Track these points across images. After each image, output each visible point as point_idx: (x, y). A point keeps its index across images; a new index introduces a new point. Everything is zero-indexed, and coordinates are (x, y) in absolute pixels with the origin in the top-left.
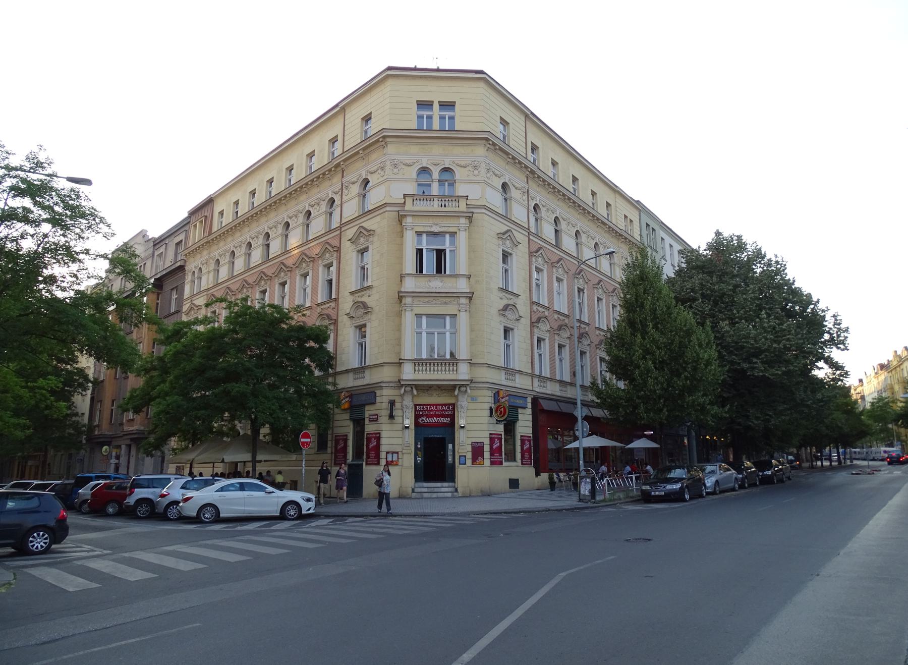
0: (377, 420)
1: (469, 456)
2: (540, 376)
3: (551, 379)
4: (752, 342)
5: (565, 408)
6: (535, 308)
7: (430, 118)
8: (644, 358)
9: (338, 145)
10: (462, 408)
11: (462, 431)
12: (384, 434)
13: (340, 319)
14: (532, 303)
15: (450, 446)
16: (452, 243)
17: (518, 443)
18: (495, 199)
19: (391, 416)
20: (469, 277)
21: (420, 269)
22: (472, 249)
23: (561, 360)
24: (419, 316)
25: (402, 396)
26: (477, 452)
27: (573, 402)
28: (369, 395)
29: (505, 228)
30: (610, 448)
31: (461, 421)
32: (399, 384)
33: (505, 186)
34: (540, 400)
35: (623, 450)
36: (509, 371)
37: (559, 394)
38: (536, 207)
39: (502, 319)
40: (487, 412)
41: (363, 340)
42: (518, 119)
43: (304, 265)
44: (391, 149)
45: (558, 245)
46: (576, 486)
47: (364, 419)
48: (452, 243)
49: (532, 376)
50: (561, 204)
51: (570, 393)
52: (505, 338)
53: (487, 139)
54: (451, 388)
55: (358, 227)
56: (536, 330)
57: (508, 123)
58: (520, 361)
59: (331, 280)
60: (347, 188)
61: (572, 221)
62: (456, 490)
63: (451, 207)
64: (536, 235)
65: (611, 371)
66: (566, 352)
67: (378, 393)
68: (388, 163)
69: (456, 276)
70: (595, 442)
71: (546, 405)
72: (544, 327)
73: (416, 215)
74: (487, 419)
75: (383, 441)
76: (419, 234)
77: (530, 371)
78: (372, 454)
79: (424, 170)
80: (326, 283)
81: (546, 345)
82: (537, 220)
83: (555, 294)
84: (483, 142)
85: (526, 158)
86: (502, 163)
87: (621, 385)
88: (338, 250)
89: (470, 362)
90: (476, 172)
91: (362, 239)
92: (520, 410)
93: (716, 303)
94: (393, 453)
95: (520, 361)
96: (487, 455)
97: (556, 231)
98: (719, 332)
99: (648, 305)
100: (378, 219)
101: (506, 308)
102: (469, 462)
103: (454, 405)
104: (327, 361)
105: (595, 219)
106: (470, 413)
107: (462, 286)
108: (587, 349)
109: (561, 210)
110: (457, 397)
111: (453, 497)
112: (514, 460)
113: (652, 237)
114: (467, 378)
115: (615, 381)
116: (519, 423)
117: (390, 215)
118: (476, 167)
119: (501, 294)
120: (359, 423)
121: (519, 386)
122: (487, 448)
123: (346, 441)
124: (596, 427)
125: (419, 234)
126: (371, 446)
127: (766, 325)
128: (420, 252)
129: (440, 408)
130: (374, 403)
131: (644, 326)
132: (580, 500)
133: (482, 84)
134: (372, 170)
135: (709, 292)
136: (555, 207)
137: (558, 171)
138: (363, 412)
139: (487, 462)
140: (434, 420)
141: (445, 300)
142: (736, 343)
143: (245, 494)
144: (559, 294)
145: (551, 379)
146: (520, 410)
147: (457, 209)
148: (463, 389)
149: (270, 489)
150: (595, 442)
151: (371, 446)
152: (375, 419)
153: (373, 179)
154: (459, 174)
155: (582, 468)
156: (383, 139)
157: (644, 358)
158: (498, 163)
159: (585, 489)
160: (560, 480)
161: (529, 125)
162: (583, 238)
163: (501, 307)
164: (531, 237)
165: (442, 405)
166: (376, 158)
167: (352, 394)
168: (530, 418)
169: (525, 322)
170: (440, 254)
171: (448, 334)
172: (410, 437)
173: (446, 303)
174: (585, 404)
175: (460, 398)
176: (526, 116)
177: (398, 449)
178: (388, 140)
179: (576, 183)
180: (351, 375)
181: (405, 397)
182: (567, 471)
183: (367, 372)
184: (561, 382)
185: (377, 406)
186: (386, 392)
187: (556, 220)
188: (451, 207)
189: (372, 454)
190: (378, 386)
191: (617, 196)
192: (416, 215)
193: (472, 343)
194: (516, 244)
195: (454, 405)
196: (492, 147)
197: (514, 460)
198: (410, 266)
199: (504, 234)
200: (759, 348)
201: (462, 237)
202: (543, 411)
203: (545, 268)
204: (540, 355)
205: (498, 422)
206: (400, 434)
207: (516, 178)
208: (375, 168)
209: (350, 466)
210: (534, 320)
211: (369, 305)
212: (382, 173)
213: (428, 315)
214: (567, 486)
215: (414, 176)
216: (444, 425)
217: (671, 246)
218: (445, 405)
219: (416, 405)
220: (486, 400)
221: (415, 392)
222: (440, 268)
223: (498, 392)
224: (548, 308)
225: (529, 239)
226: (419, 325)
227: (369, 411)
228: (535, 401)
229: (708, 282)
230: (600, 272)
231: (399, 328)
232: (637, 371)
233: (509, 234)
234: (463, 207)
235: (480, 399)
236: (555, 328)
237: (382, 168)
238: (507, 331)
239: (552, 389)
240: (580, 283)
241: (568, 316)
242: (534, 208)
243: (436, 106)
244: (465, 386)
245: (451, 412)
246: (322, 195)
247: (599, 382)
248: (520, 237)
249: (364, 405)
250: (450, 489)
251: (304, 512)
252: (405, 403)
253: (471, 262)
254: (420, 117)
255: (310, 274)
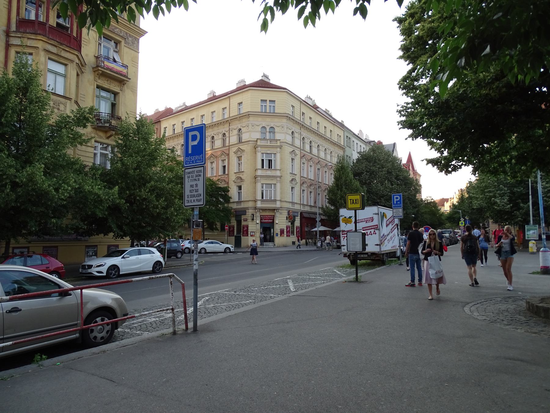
0: (247, 220)
1: (279, 233)
2: (303, 204)
3: (307, 205)
4: (381, 192)
5: (312, 216)
6: (302, 179)
7: (265, 106)
8: (341, 199)
9: (227, 111)
10: (277, 216)
11: (277, 225)
12: (249, 226)
13: (230, 182)
14: (301, 177)
15: (272, 230)
16: (275, 157)
17: (295, 229)
18: (289, 139)
19: (253, 219)
20: (280, 170)
21: (263, 167)
22: (281, 159)
23: (310, 197)
24: (262, 184)
25: (256, 212)
26: (282, 232)
27: (315, 214)
28: (244, 212)
29: (293, 149)
30: (138, 37)
31: (277, 221)
32: (255, 208)
33: (293, 132)
34: (303, 213)
35: (332, 231)
36: (293, 203)
37: (309, 211)
38: (303, 138)
39: (291, 184)
40: (286, 218)
41: (240, 191)
42: (297, 104)
43: (212, 158)
44: (251, 119)
45: (311, 153)
46: (315, 244)
47: (241, 220)
48: (275, 157)
49: (300, 204)
50: (313, 135)
51: (314, 210)
52: (292, 162)
53: (287, 116)
54: (273, 210)
55: (237, 147)
56: (302, 187)
57: (294, 107)
58: (296, 200)
59: (225, 166)
60: (232, 131)
61: (317, 141)
62: (275, 245)
63: (273, 144)
64: (303, 150)
65: (329, 203)
66: (313, 194)
67: (247, 211)
68: (250, 125)
69: (275, 170)
70: (322, 228)
71: (306, 215)
72: (305, 185)
73: (262, 146)
74: (285, 221)
75: (249, 228)
76: (263, 153)
77: (300, 203)
78: (245, 232)
79: (264, 127)
80: (222, 167)
81: (305, 192)
82: (303, 143)
83: (309, 171)
84: (286, 117)
85: (300, 121)
86: (292, 124)
87: (333, 208)
88: (228, 155)
89: (281, 201)
90: (283, 129)
91: (239, 153)
92: (296, 217)
93: (371, 174)
94: (253, 232)
95: (296, 200)
96: (285, 233)
97: (310, 146)
98: (371, 187)
99: (344, 178)
100: (246, 146)
101: (292, 180)
102: (279, 235)
103: (274, 216)
104: (227, 199)
105: (326, 139)
106: (280, 218)
107: (278, 173)
108: (320, 193)
109: (312, 137)
110: (275, 213)
111: (274, 247)
112: (294, 235)
113: (349, 141)
114: (279, 206)
115: (330, 207)
116: (296, 222)
117: (251, 146)
118: (283, 127)
119: (291, 175)
120: (239, 222)
121: (296, 208)
122: (285, 231)
123: (234, 227)
124: (323, 223)
125: (263, 153)
126: (244, 230)
127: (387, 186)
128: (263, 160)
129: (269, 216)
130: (246, 214)
131: (342, 187)
132: (317, 248)
133: (285, 94)
134: (243, 126)
135: (368, 170)
136: (310, 137)
137: (312, 121)
138: (241, 218)
139: (285, 236)
140: (266, 221)
141: (272, 178)
142: (377, 192)
143: (214, 245)
144: (310, 172)
145: (307, 205)
146: (296, 217)
147: (276, 145)
148: (278, 210)
149: (221, 243)
150: (322, 228)
151: (244, 230)
152: (246, 220)
153: (243, 130)
154: (277, 130)
155: (318, 238)
156: (248, 115)
157: (341, 199)
158: (290, 124)
159: (319, 244)
160: (309, 242)
161: (302, 105)
162: (321, 148)
163: (290, 180)
164: (301, 151)
165: (270, 216)
166: (245, 122)
167: (236, 211)
168: (299, 220)
169: (299, 184)
170: (270, 161)
171: (273, 191)
172: (259, 226)
173: (272, 180)
174: (320, 214)
175: (276, 213)
176: (301, 102)
177: (255, 231)
178: (250, 115)
179: (318, 124)
180: (235, 204)
181: (257, 213)
182: (312, 239)
183: (242, 203)
184: (311, 206)
185: (247, 215)
186: (250, 211)
187: (311, 142)
188: (273, 144)
189: (245, 232)
190: (247, 208)
191: (335, 126)
192: (262, 146)
193: (281, 193)
194: (296, 155)
195: (274, 216)
196: (289, 119)
197: (294, 235)
198: (259, 165)
199: (292, 152)
200: (384, 194)
201: (278, 155)
202: (304, 217)
203: (306, 162)
204: (303, 196)
205: (289, 222)
206: (255, 225)
207: (296, 128)
208: (245, 125)
209: (235, 236)
210: (301, 183)
211: (243, 178)
212: (248, 128)
213: (266, 184)
214: (312, 244)
215: (260, 130)
216: (270, 222)
217: (357, 144)
218: (271, 216)
219: (261, 216)
220: (285, 214)
221: (261, 211)
222: (270, 166)
223: (289, 211)
224: (306, 178)
225: (301, 152)
226: (262, 187)
227: (243, 217)
228: (301, 213)
229: (369, 165)
230: (326, 161)
231: (255, 188)
232: (338, 204)
233: (294, 151)
234: (278, 144)
235: (283, 214)
236: (309, 185)
237: (248, 126)
238: (292, 188)
239: (307, 209)
240: (319, 166)
241: (313, 180)
242: (303, 139)
243: (268, 102)
244: (279, 209)
245: (273, 218)
246: (220, 131)
247: (324, 207)
248: (298, 152)
249: (241, 215)
250: (272, 245)
251: (231, 251)
252: (257, 215)
253: (281, 163)
254: (262, 106)
255: (215, 162)
